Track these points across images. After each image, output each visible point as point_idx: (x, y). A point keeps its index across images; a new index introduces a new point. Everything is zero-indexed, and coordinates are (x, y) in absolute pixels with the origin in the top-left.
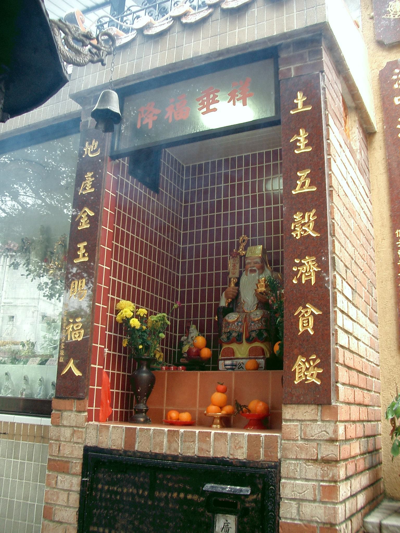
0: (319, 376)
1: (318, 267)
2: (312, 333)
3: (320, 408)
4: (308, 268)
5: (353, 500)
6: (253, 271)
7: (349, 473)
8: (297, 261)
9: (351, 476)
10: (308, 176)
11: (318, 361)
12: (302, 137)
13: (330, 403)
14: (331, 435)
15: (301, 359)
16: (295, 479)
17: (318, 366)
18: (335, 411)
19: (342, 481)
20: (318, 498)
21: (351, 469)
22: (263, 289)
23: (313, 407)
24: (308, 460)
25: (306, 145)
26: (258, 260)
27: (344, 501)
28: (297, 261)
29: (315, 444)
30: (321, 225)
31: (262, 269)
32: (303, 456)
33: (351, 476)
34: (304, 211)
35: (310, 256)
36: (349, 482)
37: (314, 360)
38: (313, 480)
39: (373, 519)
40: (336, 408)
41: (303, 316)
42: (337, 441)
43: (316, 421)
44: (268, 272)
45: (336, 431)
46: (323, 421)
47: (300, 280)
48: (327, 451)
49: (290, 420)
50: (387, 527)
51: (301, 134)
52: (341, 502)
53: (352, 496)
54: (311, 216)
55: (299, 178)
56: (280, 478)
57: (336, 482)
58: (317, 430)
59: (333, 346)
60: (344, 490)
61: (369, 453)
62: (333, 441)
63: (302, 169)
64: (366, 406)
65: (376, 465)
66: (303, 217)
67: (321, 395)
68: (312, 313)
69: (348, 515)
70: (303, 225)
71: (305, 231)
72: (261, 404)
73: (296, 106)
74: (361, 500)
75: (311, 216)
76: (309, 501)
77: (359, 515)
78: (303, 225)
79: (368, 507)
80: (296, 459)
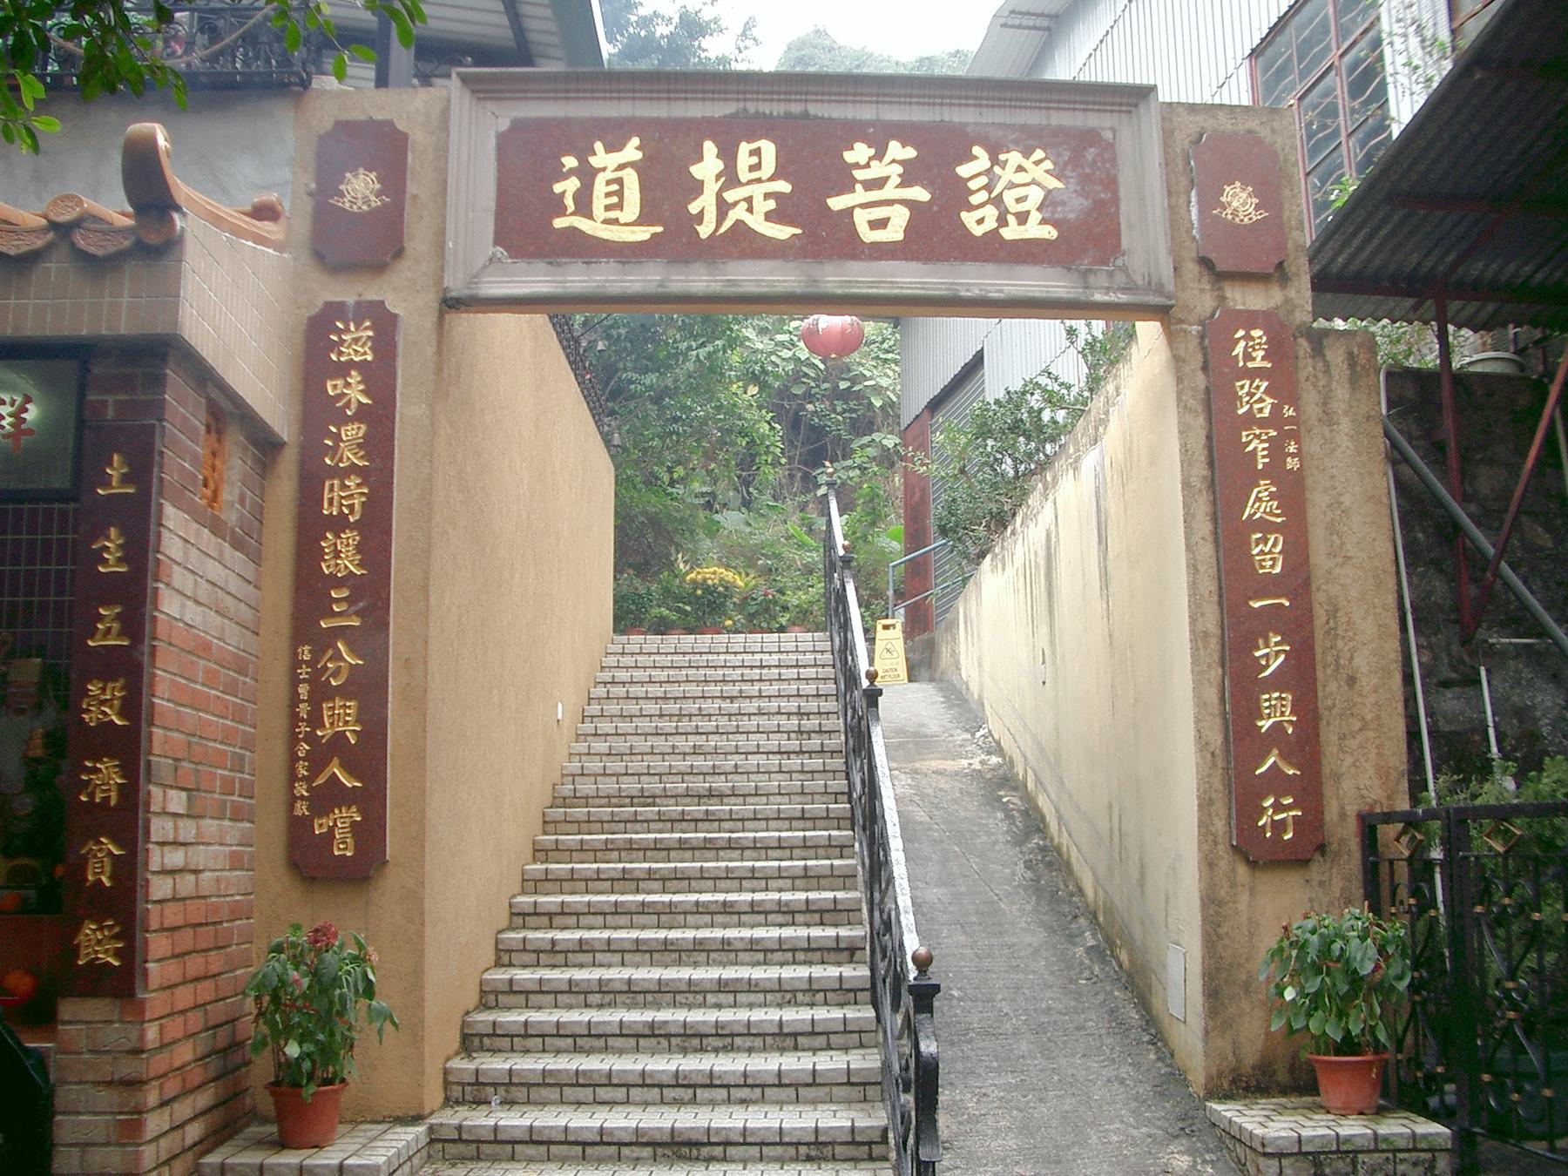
0: (118, 953)
1: (122, 777)
2: (107, 883)
3: (118, 1003)
4: (107, 777)
5: (177, 1135)
6: (21, 712)
7: (169, 1094)
8: (88, 764)
9: (174, 1099)
10: (118, 617)
11: (117, 929)
12: (112, 544)
13: (132, 994)
14: (134, 1044)
15: (89, 928)
16: (79, 1113)
17: (116, 937)
18: (141, 1007)
19: (153, 1109)
20: (113, 1138)
21: (173, 1086)
22: (39, 752)
23: (107, 1000)
24: (99, 1083)
25: (120, 561)
26: (33, 690)
27: (157, 1138)
28: (88, 764)
29: (109, 1058)
30: (133, 705)
31: (39, 707)
32: (91, 1077)
33: (174, 1099)
34: (106, 678)
35: (112, 757)
36: (167, 1110)
37: (110, 927)
38: (105, 1113)
39: (213, 1159)
40: (143, 1002)
41: (95, 856)
42: (143, 1052)
43: (112, 1022)
44: (51, 712)
45: (142, 1037)
46: (122, 1022)
47: (92, 795)
48: (128, 1068)
49: (70, 1023)
50: (232, 1167)
51: (113, 536)
52: (150, 1142)
53: (173, 1129)
54: (115, 691)
55: (101, 618)
56: (54, 1114)
57: (140, 1113)
58: (115, 1035)
59: (140, 905)
60: (155, 1123)
61: (218, 1052)
62: (137, 1052)
63: (107, 603)
64: (214, 976)
65: (238, 1068)
66: (104, 690)
67: (120, 983)
68: (110, 853)
69: (163, 1158)
70: (103, 702)
71: (105, 713)
72: (27, 980)
73: (106, 483)
74: (194, 1132)
75: (115, 691)
76: (102, 1145)
77: (190, 1155)
78: (103, 702)
79: (212, 1139)
80: (80, 1083)
